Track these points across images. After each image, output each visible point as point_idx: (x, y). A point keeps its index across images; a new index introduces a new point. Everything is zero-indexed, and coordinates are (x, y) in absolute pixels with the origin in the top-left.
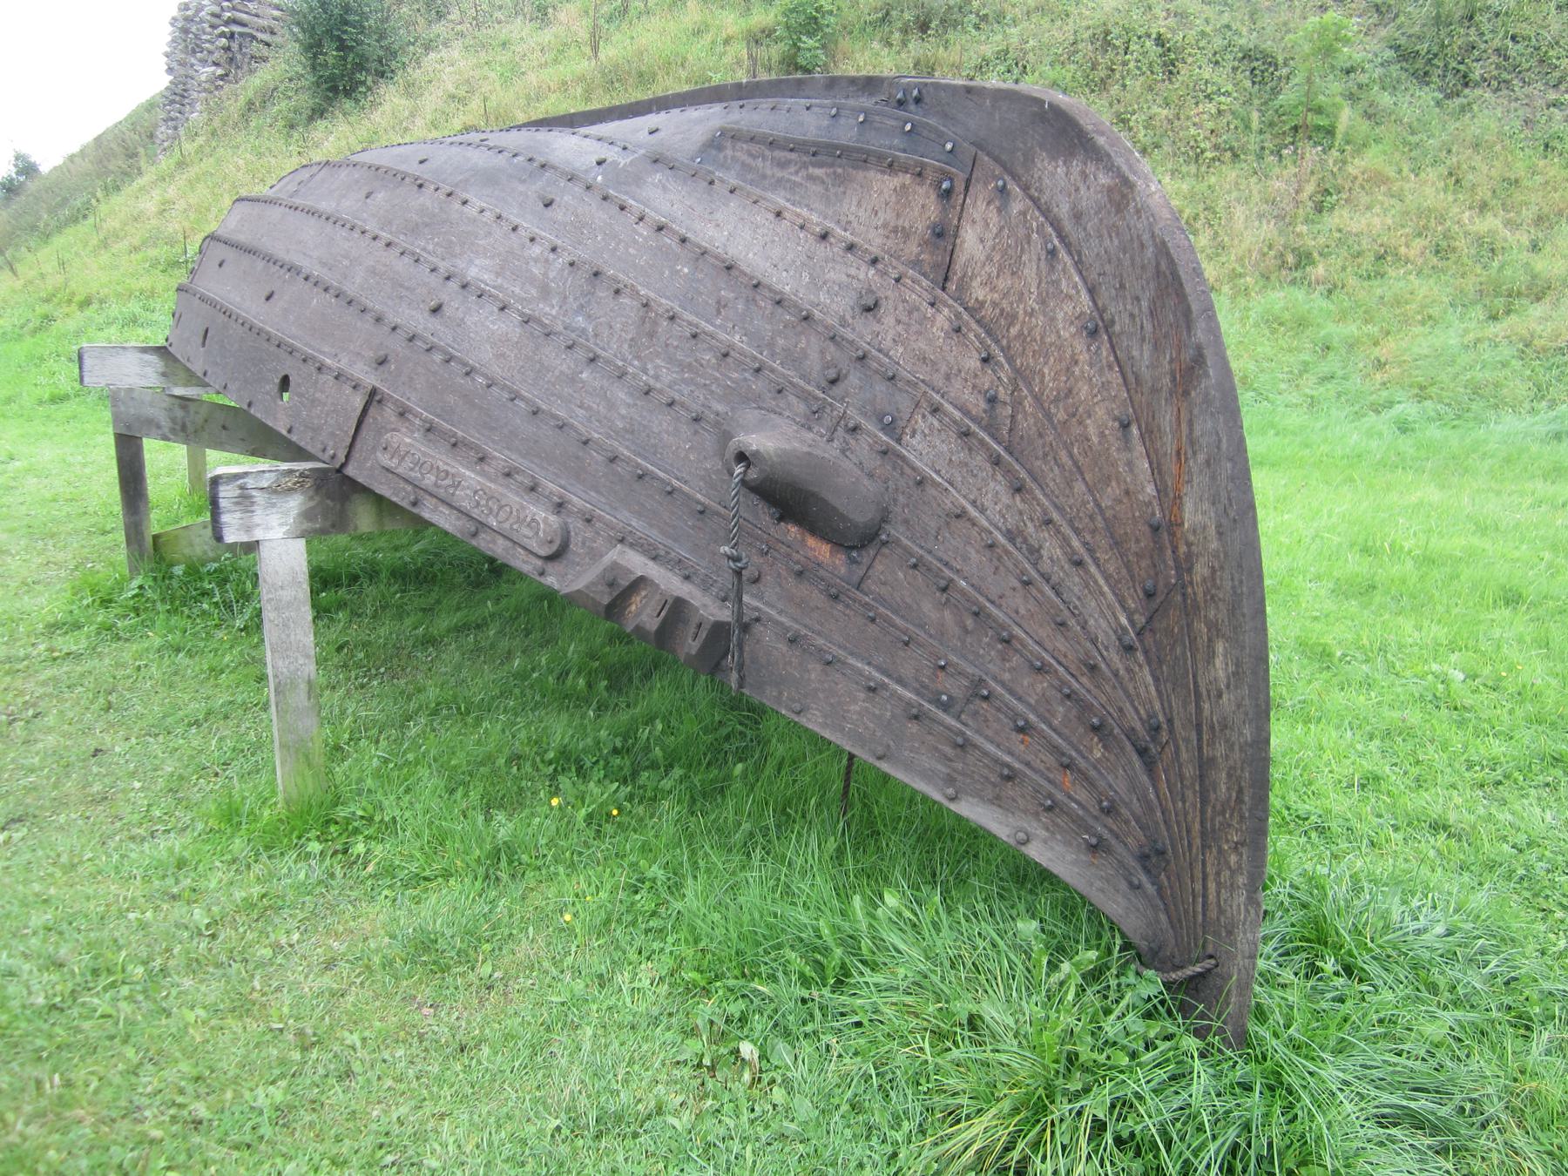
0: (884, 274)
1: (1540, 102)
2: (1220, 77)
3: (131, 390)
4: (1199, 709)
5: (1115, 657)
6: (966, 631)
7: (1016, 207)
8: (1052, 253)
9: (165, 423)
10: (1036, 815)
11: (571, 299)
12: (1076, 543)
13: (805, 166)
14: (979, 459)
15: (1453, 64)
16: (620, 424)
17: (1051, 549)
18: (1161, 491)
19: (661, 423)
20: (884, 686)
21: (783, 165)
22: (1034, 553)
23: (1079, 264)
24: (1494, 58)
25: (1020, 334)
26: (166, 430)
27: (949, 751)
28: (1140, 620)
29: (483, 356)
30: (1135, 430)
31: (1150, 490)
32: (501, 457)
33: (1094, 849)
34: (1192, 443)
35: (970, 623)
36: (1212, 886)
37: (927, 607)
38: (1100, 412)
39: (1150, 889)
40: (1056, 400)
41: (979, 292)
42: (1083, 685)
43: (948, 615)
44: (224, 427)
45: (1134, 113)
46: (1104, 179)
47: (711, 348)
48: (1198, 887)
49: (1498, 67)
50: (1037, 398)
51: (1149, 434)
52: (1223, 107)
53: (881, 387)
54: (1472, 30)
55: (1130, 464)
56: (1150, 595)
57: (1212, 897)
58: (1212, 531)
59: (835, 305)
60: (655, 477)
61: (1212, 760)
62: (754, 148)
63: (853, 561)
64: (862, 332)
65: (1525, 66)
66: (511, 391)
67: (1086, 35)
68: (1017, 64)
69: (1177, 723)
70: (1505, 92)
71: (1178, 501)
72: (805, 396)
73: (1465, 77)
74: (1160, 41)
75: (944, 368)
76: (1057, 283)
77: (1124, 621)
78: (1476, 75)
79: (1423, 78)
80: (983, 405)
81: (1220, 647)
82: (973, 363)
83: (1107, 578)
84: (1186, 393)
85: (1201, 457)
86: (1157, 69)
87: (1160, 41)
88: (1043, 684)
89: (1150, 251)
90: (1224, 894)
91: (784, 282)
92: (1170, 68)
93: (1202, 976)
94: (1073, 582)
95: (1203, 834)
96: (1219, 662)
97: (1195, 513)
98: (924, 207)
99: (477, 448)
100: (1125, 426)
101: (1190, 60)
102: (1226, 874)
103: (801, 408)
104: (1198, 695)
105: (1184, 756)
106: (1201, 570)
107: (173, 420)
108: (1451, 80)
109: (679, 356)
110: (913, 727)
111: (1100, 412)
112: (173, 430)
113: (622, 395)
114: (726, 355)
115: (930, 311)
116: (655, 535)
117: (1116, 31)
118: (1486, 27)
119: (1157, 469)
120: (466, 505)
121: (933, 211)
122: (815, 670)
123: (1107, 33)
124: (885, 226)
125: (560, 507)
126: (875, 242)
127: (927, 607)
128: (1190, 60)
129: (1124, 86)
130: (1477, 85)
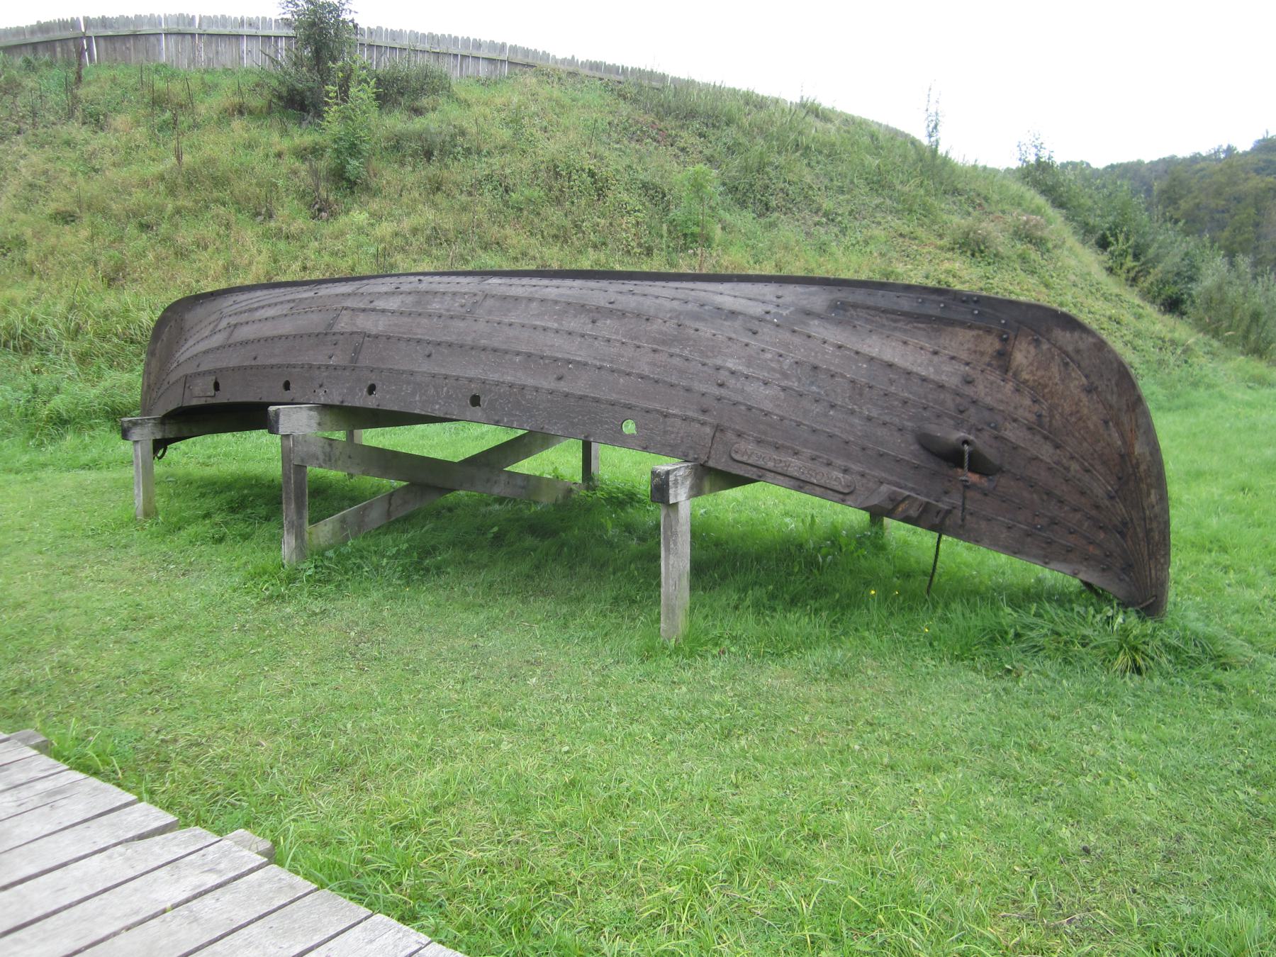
0: (974, 369)
1: (810, 222)
2: (632, 200)
3: (304, 436)
4: (1144, 513)
5: (1107, 503)
6: (1043, 500)
7: (1045, 346)
8: (1066, 364)
9: (321, 457)
10: (1081, 563)
11: (804, 379)
12: (1086, 464)
13: (910, 322)
14: (1037, 438)
15: (759, 196)
16: (859, 434)
17: (1074, 466)
18: (1124, 442)
19: (881, 432)
20: (1015, 526)
21: (895, 321)
22: (1068, 469)
23: (1079, 367)
24: (781, 195)
25: (1050, 392)
26: (321, 461)
27: (1044, 545)
28: (1116, 487)
29: (768, 406)
30: (1111, 424)
31: (1119, 443)
32: (808, 452)
33: (1103, 570)
34: (1137, 426)
35: (1045, 497)
36: (1153, 572)
37: (1025, 494)
38: (1094, 418)
39: (1127, 579)
40: (1071, 414)
41: (1025, 376)
42: (1094, 513)
43: (1035, 496)
44: (350, 457)
45: (583, 222)
46: (1091, 340)
47: (897, 399)
48: (1147, 573)
49: (784, 200)
50: (1062, 414)
51: (1117, 424)
52: (640, 220)
53: (986, 414)
54: (765, 177)
55: (1109, 435)
56: (1120, 479)
57: (1153, 575)
58: (1148, 454)
59: (953, 381)
60: (888, 455)
61: (1151, 530)
62: (872, 312)
63: (990, 480)
64: (969, 390)
65: (798, 200)
66: (796, 422)
67: (543, 167)
68: (501, 185)
69: (1135, 520)
70: (790, 215)
71: (1132, 445)
72: (952, 418)
73: (766, 204)
74: (592, 174)
75: (1013, 405)
76: (1070, 374)
77: (1110, 488)
78: (773, 203)
79: (743, 204)
80: (1035, 417)
81: (1153, 491)
82: (1028, 402)
83: (1101, 474)
84: (1134, 411)
85: (1142, 431)
86: (592, 192)
87: (592, 174)
88: (1078, 516)
89: (1115, 365)
90: (1159, 573)
91: (928, 372)
92: (601, 193)
93: (1151, 604)
94: (1086, 478)
95: (1149, 555)
96: (1152, 496)
97: (1139, 449)
98: (991, 344)
99: (792, 449)
100: (1106, 423)
101: (613, 188)
102: (1159, 567)
103: (952, 422)
104: (1143, 508)
105: (1138, 530)
106: (1143, 467)
107: (324, 453)
108: (760, 207)
109: (879, 403)
110: (1029, 539)
111: (1094, 418)
112: (324, 460)
113: (857, 421)
114: (906, 403)
115: (1002, 383)
116: (894, 478)
117: (562, 166)
118: (773, 174)
119: (1122, 435)
120: (796, 474)
121: (997, 345)
122: (983, 524)
123: (556, 167)
124: (969, 349)
125: (846, 471)
126: (964, 356)
127: (1025, 494)
128: (613, 188)
129: (573, 203)
130: (774, 210)
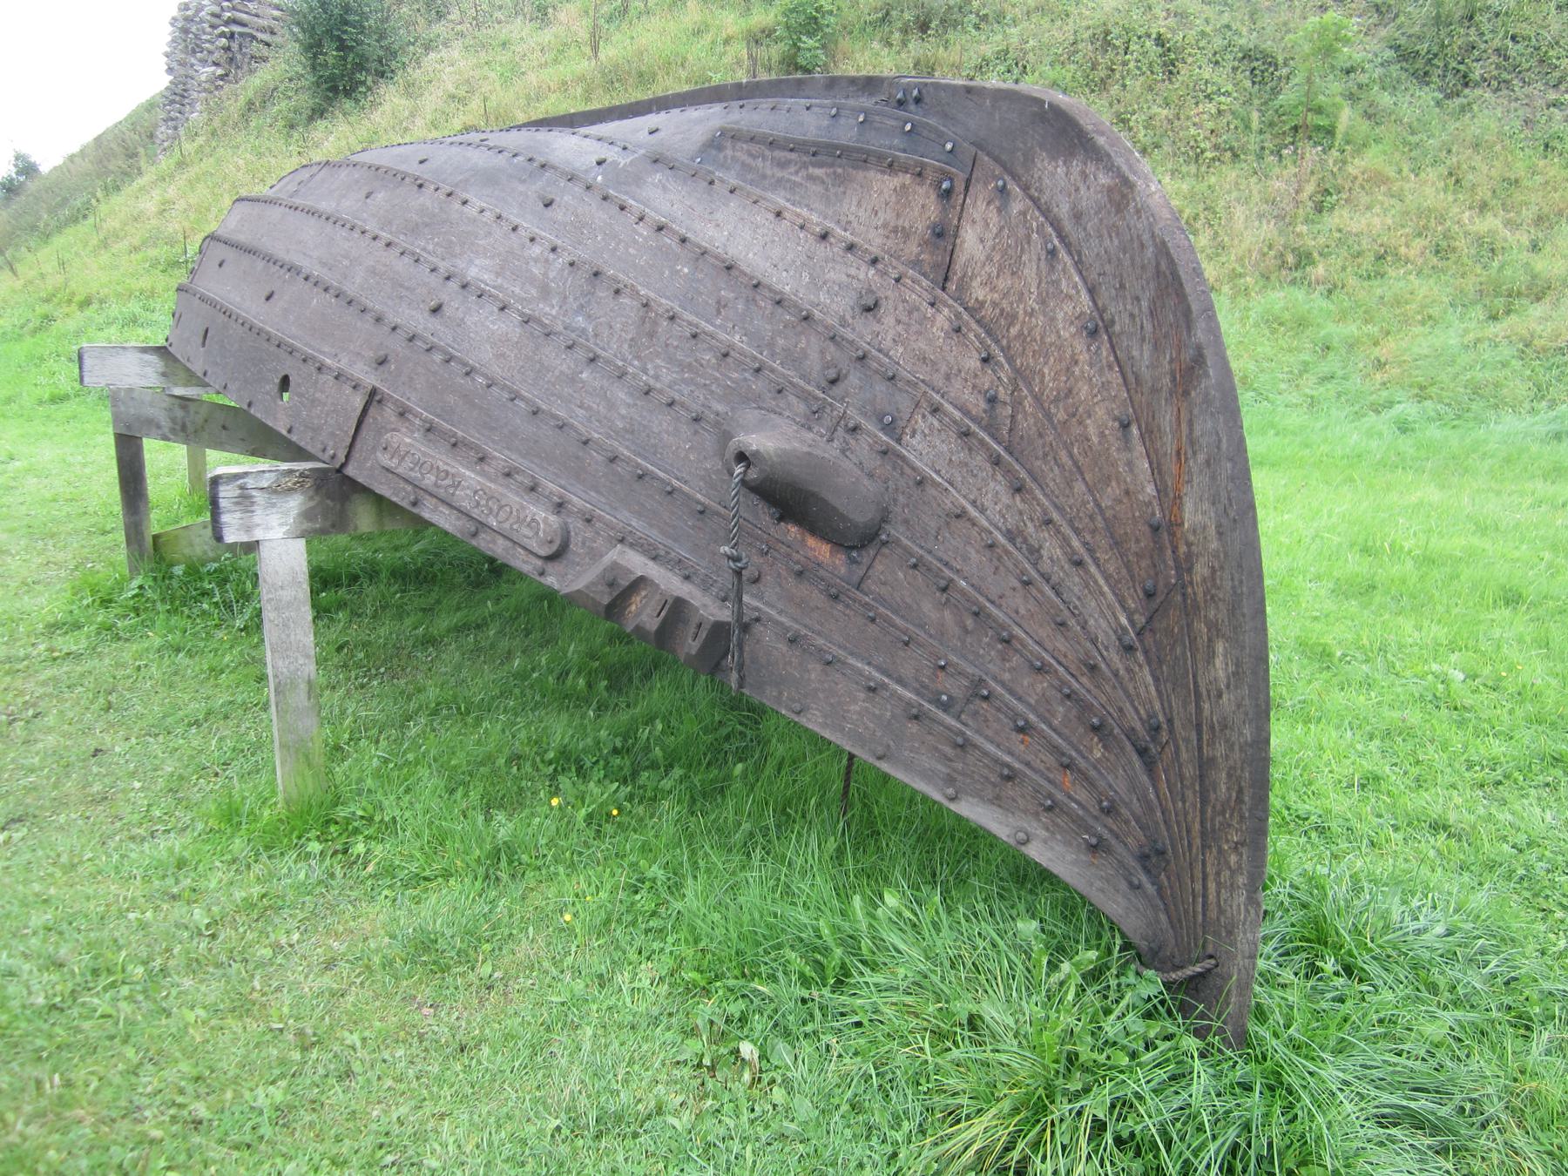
0: (884, 274)
1: (1540, 102)
2: (1220, 77)
3: (131, 390)
4: (1199, 709)
5: (1115, 657)
6: (966, 631)
7: (1016, 207)
8: (1052, 253)
9: (165, 423)
10: (1036, 815)
11: (571, 299)
12: (1076, 543)
13: (805, 166)
14: (979, 459)
15: (1453, 64)
16: (620, 424)
17: (1051, 549)
18: (1161, 491)
19: (661, 423)
20: (884, 686)
21: (783, 165)
22: (1034, 553)
23: (1079, 264)
24: (1494, 58)
25: (1020, 334)
26: (166, 430)
27: (949, 751)
28: (1140, 620)
29: (483, 356)
30: (1135, 430)
31: (1150, 490)
32: (501, 457)
33: (1094, 849)
34: (1192, 443)
35: (970, 623)
36: (1212, 886)
37: (927, 607)
38: (1100, 412)
39: (1150, 889)
40: (1056, 400)
41: (979, 292)
42: (1083, 685)
43: (948, 615)
44: (224, 427)
45: (1134, 113)
46: (1104, 179)
47: (711, 348)
48: (1198, 887)
49: (1498, 67)
50: (1037, 398)
51: (1149, 434)
52: (1223, 107)
53: (881, 387)
54: (1472, 30)
55: (1130, 464)
56: (1150, 595)
57: (1212, 897)
58: (1212, 531)
59: (835, 305)
60: (655, 477)
61: (1212, 760)
62: (754, 148)
63: (853, 561)
64: (862, 332)
65: (1525, 66)
66: (511, 391)
67: (1086, 35)
68: (1017, 64)
69: (1177, 723)
70: (1505, 92)
71: (1178, 501)
72: (805, 396)
73: (1465, 77)
74: (1160, 41)
75: (944, 368)
76: (1057, 283)
77: (1124, 621)
78: (1476, 75)
79: (1423, 78)
80: (983, 405)
81: (1220, 647)
82: (973, 363)
83: (1107, 578)
84: (1186, 393)
85: (1201, 457)
86: (1157, 69)
87: (1160, 41)
88: (1043, 684)
89: (1150, 251)
90: (1224, 894)
91: (784, 282)
92: (1170, 68)
93: (1202, 976)
94: (1073, 582)
95: (1203, 834)
96: (1219, 662)
97: (1195, 513)
98: (924, 207)
99: (477, 448)
100: (1125, 426)
101: (1190, 60)
102: (1226, 874)
103: (801, 408)
104: (1198, 695)
105: (1184, 756)
106: (1201, 570)
107: (173, 420)
108: (1451, 80)
109: (679, 356)
110: (913, 727)
111: (1100, 412)
112: (173, 430)
113: (622, 395)
114: (726, 355)
115: (930, 311)
116: (655, 535)
117: (1116, 31)
118: (1486, 27)
119: (1157, 469)
120: (466, 505)
121: (933, 211)
122: (815, 670)
123: (1107, 33)
124: (885, 226)
125: (560, 507)
126: (875, 242)
127: (927, 607)
128: (1190, 60)
129: (1124, 86)
130: (1477, 85)
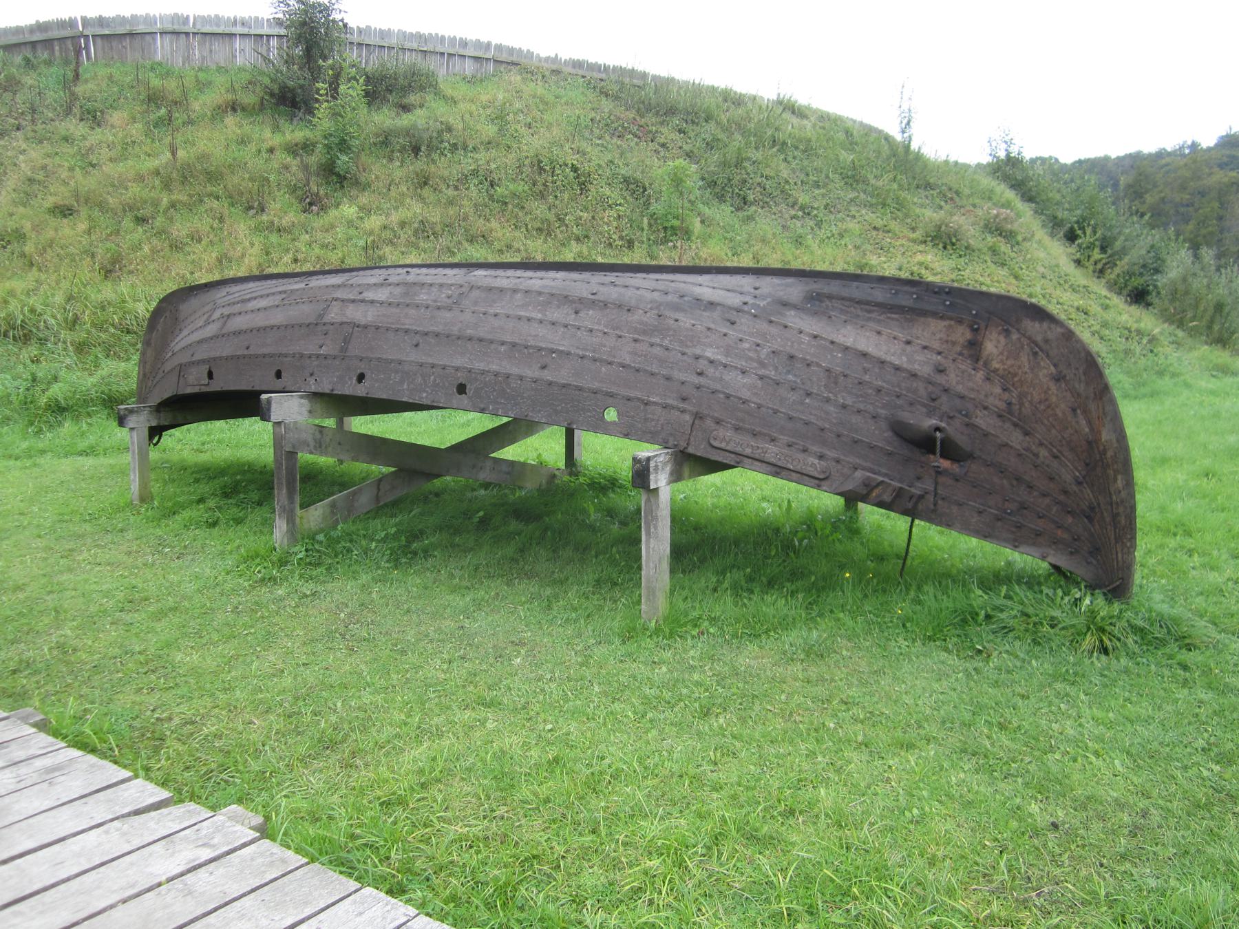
0: (946, 358)
1: (787, 216)
2: (614, 194)
3: (296, 423)
4: (1111, 498)
5: (1075, 488)
6: (1013, 486)
7: (1015, 336)
8: (1035, 354)
9: (312, 443)
10: (1050, 546)
11: (780, 368)
12: (1055, 450)
13: (884, 313)
14: (1007, 425)
15: (737, 191)
16: (834, 421)
17: (1043, 453)
18: (1092, 429)
19: (856, 420)
20: (985, 510)
21: (870, 312)
22: (1037, 455)
23: (1048, 356)
24: (758, 189)
25: (1020, 380)
26: (312, 447)
27: (1014, 529)
28: (1084, 473)
29: (746, 394)
30: (1079, 411)
31: (1087, 430)
32: (784, 439)
33: (1071, 553)
34: (1104, 414)
35: (1015, 483)
36: (1120, 555)
37: (996, 480)
38: (1063, 406)
39: (1095, 562)
40: (1040, 402)
41: (995, 365)
42: (1062, 498)
43: (1005, 482)
44: (340, 444)
45: (566, 215)
46: (1059, 330)
47: (871, 388)
48: (1114, 556)
49: (761, 194)
50: (1031, 402)
51: (1085, 412)
52: (621, 213)
53: (958, 401)
54: (743, 172)
55: (1077, 422)
56: (1087, 465)
57: (1120, 558)
58: (1114, 440)
59: (925, 370)
60: (863, 441)
61: (1118, 514)
62: (847, 303)
63: (961, 466)
64: (941, 379)
65: (775, 194)
66: (773, 409)
67: (527, 162)
68: (486, 179)
69: (1102, 505)
70: (767, 209)
71: (1100, 432)
72: (924, 405)
73: (744, 199)
74: (574, 169)
75: (983, 393)
76: (1039, 363)
77: (1077, 474)
78: (751, 198)
79: (721, 198)
80: (1005, 405)
81: (1119, 477)
82: (998, 390)
83: (1069, 461)
84: (1101, 399)
85: (1109, 418)
86: (575, 187)
87: (574, 169)
88: (1047, 501)
89: (1083, 354)
90: (1125, 556)
91: (902, 361)
92: (583, 187)
93: (1118, 586)
94: (1055, 464)
95: (1116, 538)
96: (1119, 482)
97: (1106, 436)
98: (962, 334)
99: (769, 435)
100: (1074, 410)
101: (595, 182)
102: (1125, 550)
103: (924, 410)
104: (1110, 493)
105: (1105, 514)
106: (1110, 454)
107: (315, 440)
108: (738, 201)
109: (854, 391)
110: (999, 524)
111: (1063, 406)
112: (315, 447)
113: (832, 409)
114: (879, 391)
115: (973, 372)
116: (868, 464)
117: (545, 161)
118: (750, 169)
119: (1089, 423)
120: (773, 460)
121: (969, 335)
122: (955, 509)
123: (540, 162)
124: (941, 339)
125: (821, 457)
126: (936, 345)
127: (996, 480)
128: (595, 182)
129: (556, 197)
130: (752, 204)
